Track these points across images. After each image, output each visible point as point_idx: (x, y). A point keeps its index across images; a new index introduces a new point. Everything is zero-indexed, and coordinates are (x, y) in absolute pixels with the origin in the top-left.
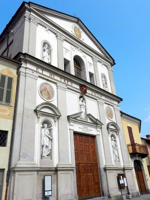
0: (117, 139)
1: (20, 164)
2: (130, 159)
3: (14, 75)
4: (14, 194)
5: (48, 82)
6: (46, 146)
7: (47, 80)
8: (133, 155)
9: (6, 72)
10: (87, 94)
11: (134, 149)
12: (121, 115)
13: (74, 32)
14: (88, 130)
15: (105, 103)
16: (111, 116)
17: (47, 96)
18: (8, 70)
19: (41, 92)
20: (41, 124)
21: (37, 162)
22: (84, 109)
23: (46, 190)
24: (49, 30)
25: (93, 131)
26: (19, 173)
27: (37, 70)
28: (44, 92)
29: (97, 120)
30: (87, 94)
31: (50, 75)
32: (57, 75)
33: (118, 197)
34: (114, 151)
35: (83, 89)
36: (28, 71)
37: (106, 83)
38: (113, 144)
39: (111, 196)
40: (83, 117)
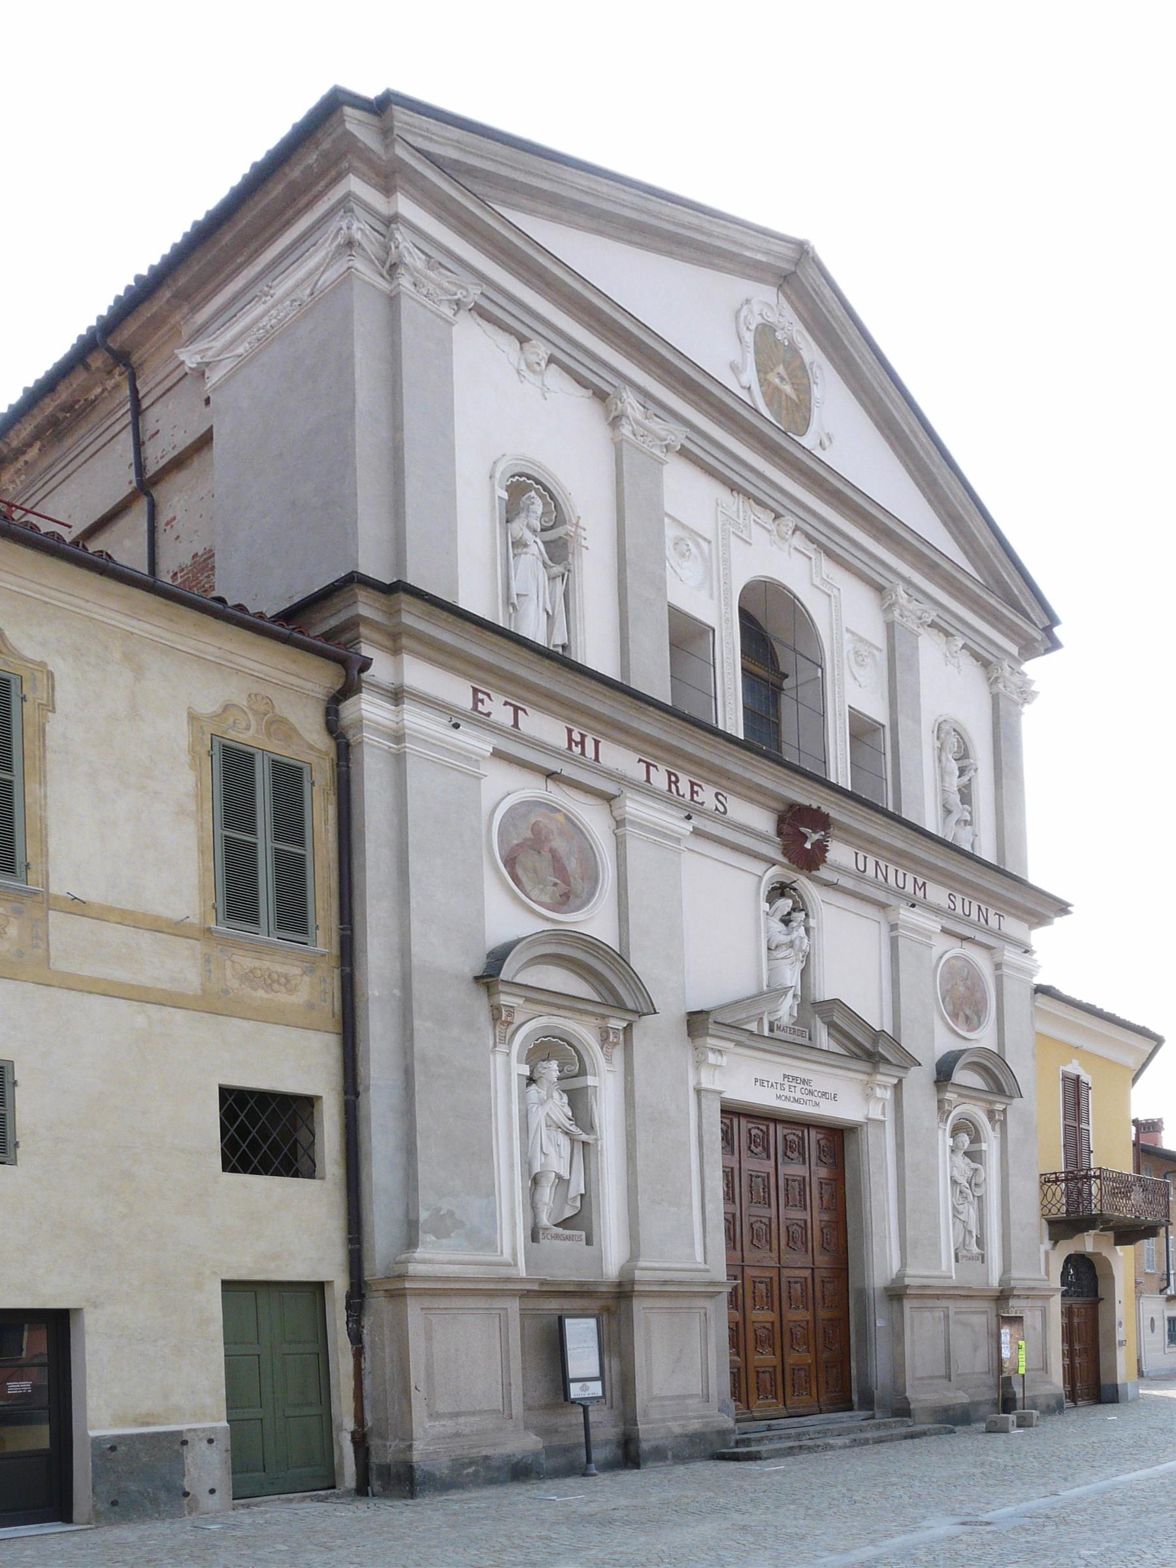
0: (991, 1145)
1: (423, 1262)
2: (1047, 1244)
3: (311, 747)
4: (413, 1388)
5: (557, 795)
6: (559, 1177)
7: (550, 775)
8: (1062, 1228)
9: (253, 723)
10: (824, 873)
13: (750, 376)
14: (811, 1093)
16: (968, 1012)
17: (550, 888)
18: (262, 708)
19: (511, 862)
20: (519, 1062)
21: (510, 1247)
22: (799, 966)
23: (571, 1375)
24: (552, 360)
25: (840, 1097)
26: (427, 1302)
27: (475, 708)
28: (528, 859)
29: (878, 1035)
31: (570, 740)
32: (624, 738)
33: (951, 1413)
34: (960, 1208)
36: (414, 718)
37: (966, 795)
38: (956, 1173)
39: (912, 1407)
40: (786, 1020)
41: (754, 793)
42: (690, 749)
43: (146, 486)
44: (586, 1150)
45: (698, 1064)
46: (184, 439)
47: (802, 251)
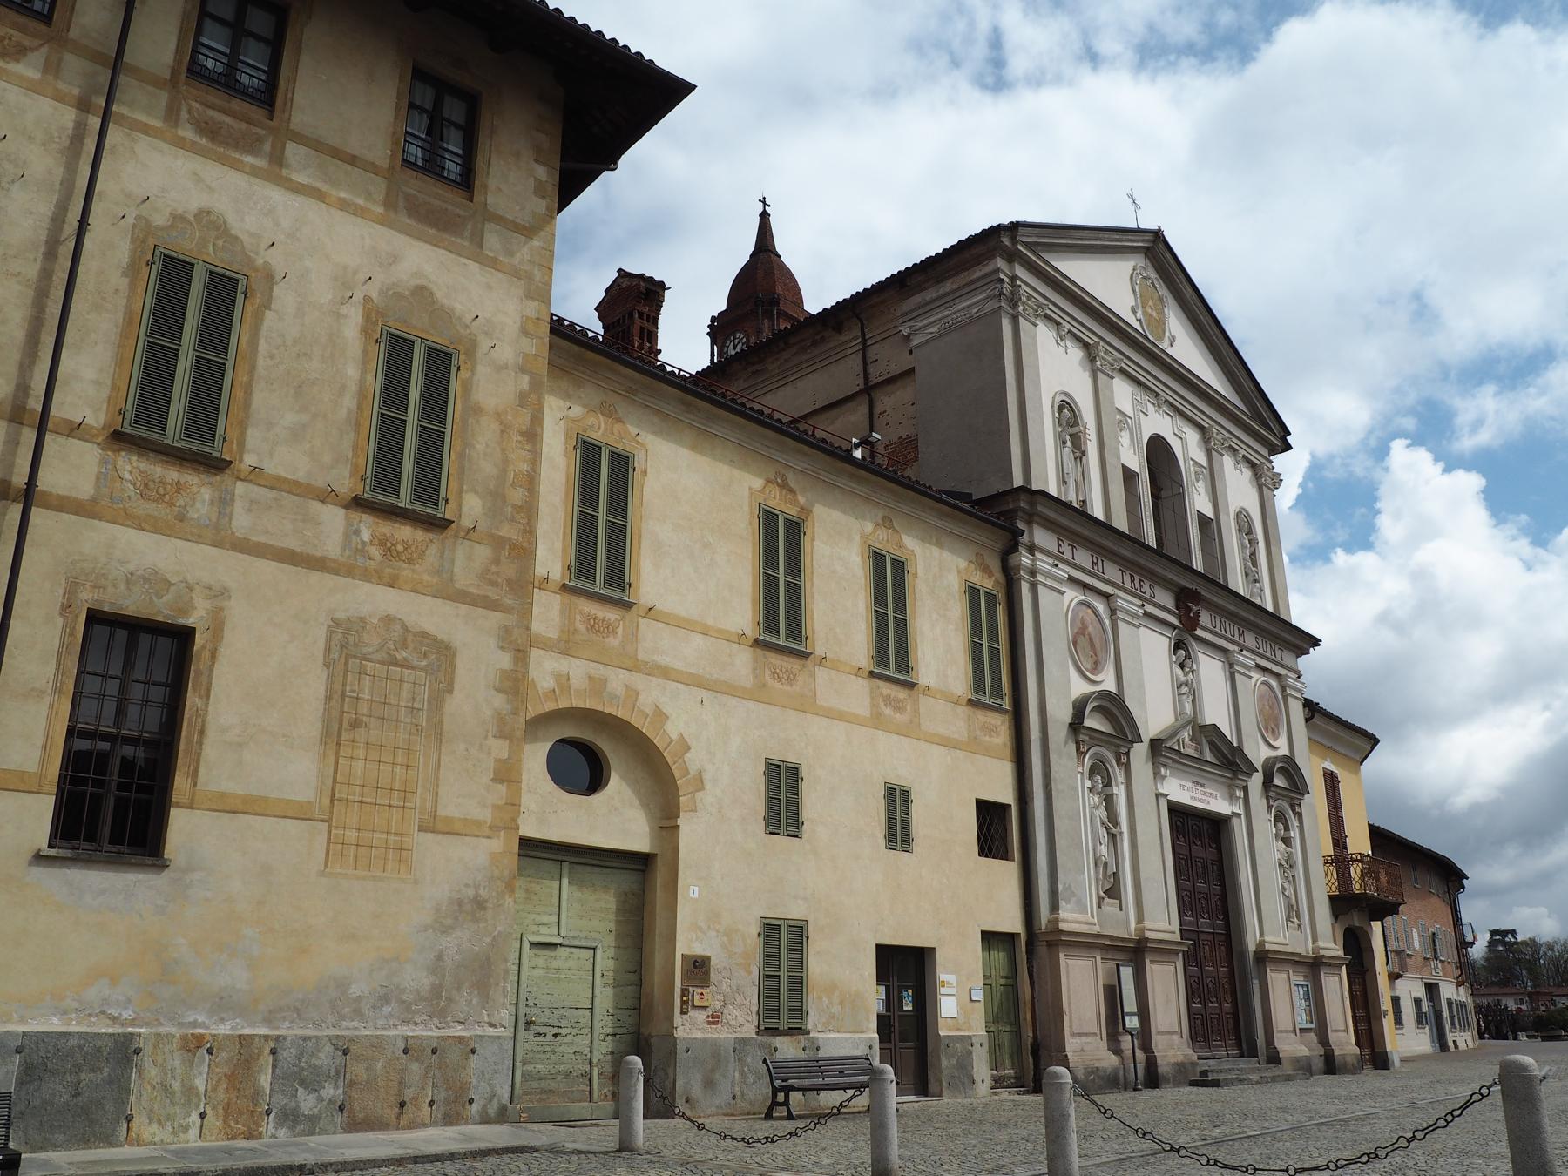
11: (1344, 879)
12: (1307, 720)
15: (1258, 666)
30: (1199, 632)
35: (1190, 609)
37: (1255, 564)
41: (1166, 584)
42: (1142, 561)
43: (869, 390)
44: (1113, 837)
45: (1156, 774)
46: (895, 369)
47: (1157, 235)
